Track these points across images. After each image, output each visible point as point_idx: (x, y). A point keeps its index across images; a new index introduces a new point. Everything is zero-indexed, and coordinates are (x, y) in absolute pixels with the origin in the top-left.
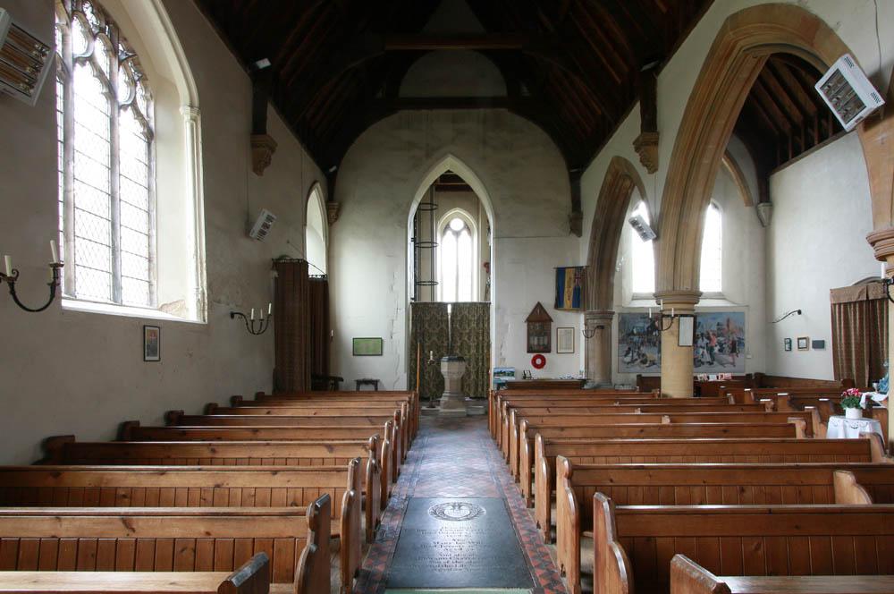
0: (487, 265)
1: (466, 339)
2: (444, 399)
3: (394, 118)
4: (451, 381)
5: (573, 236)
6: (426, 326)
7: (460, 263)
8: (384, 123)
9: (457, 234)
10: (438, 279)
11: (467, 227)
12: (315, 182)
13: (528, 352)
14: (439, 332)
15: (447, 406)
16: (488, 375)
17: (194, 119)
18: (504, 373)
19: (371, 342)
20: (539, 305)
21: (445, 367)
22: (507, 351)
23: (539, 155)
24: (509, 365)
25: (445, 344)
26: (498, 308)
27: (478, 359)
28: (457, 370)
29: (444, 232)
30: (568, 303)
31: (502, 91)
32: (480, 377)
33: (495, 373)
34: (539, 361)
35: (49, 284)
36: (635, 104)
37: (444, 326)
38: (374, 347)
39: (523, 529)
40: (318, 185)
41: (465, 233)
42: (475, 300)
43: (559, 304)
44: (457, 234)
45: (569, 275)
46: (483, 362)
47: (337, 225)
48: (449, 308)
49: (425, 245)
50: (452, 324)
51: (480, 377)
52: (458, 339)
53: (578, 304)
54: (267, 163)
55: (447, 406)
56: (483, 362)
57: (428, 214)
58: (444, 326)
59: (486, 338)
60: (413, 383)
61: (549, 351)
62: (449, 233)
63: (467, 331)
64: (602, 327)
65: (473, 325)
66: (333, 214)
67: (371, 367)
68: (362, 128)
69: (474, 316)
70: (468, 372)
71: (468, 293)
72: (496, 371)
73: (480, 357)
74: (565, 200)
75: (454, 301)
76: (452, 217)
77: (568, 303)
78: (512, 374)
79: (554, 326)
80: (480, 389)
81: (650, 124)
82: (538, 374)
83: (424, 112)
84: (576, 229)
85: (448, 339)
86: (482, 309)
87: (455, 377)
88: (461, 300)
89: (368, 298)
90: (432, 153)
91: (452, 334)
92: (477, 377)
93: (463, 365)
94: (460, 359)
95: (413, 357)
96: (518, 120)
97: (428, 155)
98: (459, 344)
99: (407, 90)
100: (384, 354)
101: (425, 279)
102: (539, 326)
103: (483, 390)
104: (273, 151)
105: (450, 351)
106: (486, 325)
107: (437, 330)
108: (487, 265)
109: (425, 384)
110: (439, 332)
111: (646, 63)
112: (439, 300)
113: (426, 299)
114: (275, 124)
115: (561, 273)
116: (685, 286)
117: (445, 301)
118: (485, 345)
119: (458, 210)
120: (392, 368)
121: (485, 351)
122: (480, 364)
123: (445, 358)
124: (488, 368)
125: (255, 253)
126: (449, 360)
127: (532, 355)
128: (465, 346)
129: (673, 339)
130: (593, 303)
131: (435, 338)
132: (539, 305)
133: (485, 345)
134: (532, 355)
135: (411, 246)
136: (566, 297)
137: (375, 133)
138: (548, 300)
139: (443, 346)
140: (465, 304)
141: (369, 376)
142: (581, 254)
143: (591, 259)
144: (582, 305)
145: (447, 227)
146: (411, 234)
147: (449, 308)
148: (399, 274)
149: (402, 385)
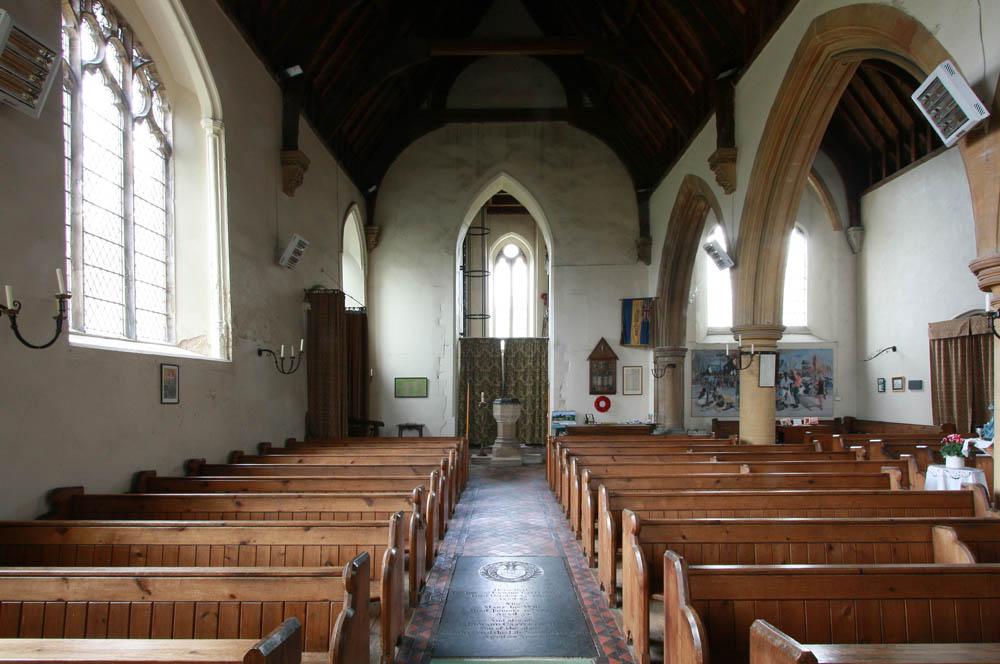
0: (544, 297)
1: (521, 379)
2: (496, 446)
3: (441, 132)
4: (504, 426)
5: (641, 264)
6: (477, 364)
7: (514, 294)
8: (429, 137)
9: (511, 261)
10: (490, 312)
11: (523, 254)
12: (352, 204)
13: (591, 393)
14: (491, 371)
15: (500, 453)
16: (546, 419)
17: (217, 133)
18: (563, 417)
19: (415, 382)
20: (603, 341)
21: (498, 411)
22: (567, 392)
23: (603, 174)
24: (569, 408)
25: (498, 385)
26: (557, 344)
27: (535, 401)
28: (511, 414)
29: (497, 260)
30: (635, 338)
31: (562, 102)
32: (537, 421)
33: (553, 418)
34: (602, 404)
35: (55, 318)
36: (710, 116)
37: (496, 364)
38: (419, 388)
39: (585, 591)
40: (356, 207)
41: (520, 260)
42: (531, 336)
43: (625, 340)
44: (511, 261)
45: (637, 308)
46: (540, 405)
47: (378, 252)
48: (503, 344)
49: (475, 274)
50: (506, 363)
51: (537, 421)
52: (512, 379)
53: (647, 340)
54: (299, 183)
55: (500, 453)
56: (540, 405)
57: (479, 239)
58: (496, 364)
59: (543, 378)
60: (462, 428)
61: (614, 393)
62: (502, 260)
63: (523, 370)
64: (673, 366)
65: (529, 363)
66: (372, 239)
67: (415, 410)
68: (405, 143)
69: (531, 353)
70: (524, 416)
71: (524, 328)
72: (555, 414)
73: (537, 399)
74: (632, 223)
75: (508, 336)
76: (506, 243)
77: (635, 338)
78: (573, 418)
79: (619, 364)
80: (537, 435)
81: (727, 138)
82: (601, 418)
83: (474, 125)
84: (644, 256)
85: (501, 379)
86: (539, 345)
87: (509, 421)
88: (516, 335)
89: (411, 333)
90: (483, 172)
91: (506, 374)
92: (534, 421)
93: (518, 407)
94: (515, 401)
95: (462, 399)
96: (580, 135)
97: (479, 174)
98: (513, 385)
99: (455, 101)
100: (430, 396)
101: (475, 312)
102: (603, 365)
103: (540, 436)
104: (305, 168)
105: (503, 393)
106: (543, 364)
107: (489, 369)
108: (544, 297)
109: (475, 430)
110: (491, 371)
111: (723, 71)
112: (491, 335)
113: (476, 334)
114: (308, 138)
115: (627, 305)
116: (767, 320)
117: (498, 336)
118: (543, 385)
119: (512, 235)
120: (438, 412)
121: (543, 393)
122: (537, 407)
123: (498, 400)
124: (546, 412)
125: (285, 282)
126: (503, 402)
127: (595, 397)
128: (520, 387)
129: (753, 379)
130: (663, 339)
131: (486, 378)
132: (603, 341)
133: (543, 385)
134: (595, 397)
135: (459, 275)
136: (633, 332)
137: (419, 149)
138: (613, 336)
139: (495, 387)
140: (520, 339)
141: (413, 421)
142: (650, 283)
143: (661, 290)
144: (650, 341)
145: (500, 254)
146: (459, 262)
147: (503, 344)
148: (447, 307)
149: (450, 430)
